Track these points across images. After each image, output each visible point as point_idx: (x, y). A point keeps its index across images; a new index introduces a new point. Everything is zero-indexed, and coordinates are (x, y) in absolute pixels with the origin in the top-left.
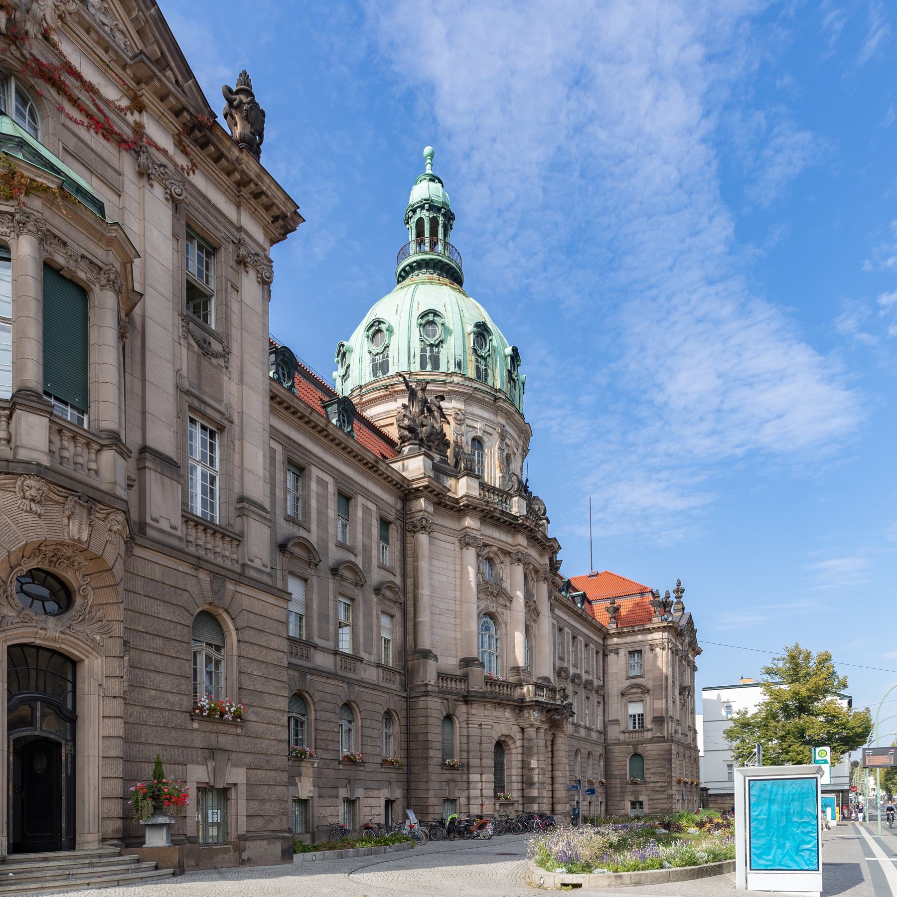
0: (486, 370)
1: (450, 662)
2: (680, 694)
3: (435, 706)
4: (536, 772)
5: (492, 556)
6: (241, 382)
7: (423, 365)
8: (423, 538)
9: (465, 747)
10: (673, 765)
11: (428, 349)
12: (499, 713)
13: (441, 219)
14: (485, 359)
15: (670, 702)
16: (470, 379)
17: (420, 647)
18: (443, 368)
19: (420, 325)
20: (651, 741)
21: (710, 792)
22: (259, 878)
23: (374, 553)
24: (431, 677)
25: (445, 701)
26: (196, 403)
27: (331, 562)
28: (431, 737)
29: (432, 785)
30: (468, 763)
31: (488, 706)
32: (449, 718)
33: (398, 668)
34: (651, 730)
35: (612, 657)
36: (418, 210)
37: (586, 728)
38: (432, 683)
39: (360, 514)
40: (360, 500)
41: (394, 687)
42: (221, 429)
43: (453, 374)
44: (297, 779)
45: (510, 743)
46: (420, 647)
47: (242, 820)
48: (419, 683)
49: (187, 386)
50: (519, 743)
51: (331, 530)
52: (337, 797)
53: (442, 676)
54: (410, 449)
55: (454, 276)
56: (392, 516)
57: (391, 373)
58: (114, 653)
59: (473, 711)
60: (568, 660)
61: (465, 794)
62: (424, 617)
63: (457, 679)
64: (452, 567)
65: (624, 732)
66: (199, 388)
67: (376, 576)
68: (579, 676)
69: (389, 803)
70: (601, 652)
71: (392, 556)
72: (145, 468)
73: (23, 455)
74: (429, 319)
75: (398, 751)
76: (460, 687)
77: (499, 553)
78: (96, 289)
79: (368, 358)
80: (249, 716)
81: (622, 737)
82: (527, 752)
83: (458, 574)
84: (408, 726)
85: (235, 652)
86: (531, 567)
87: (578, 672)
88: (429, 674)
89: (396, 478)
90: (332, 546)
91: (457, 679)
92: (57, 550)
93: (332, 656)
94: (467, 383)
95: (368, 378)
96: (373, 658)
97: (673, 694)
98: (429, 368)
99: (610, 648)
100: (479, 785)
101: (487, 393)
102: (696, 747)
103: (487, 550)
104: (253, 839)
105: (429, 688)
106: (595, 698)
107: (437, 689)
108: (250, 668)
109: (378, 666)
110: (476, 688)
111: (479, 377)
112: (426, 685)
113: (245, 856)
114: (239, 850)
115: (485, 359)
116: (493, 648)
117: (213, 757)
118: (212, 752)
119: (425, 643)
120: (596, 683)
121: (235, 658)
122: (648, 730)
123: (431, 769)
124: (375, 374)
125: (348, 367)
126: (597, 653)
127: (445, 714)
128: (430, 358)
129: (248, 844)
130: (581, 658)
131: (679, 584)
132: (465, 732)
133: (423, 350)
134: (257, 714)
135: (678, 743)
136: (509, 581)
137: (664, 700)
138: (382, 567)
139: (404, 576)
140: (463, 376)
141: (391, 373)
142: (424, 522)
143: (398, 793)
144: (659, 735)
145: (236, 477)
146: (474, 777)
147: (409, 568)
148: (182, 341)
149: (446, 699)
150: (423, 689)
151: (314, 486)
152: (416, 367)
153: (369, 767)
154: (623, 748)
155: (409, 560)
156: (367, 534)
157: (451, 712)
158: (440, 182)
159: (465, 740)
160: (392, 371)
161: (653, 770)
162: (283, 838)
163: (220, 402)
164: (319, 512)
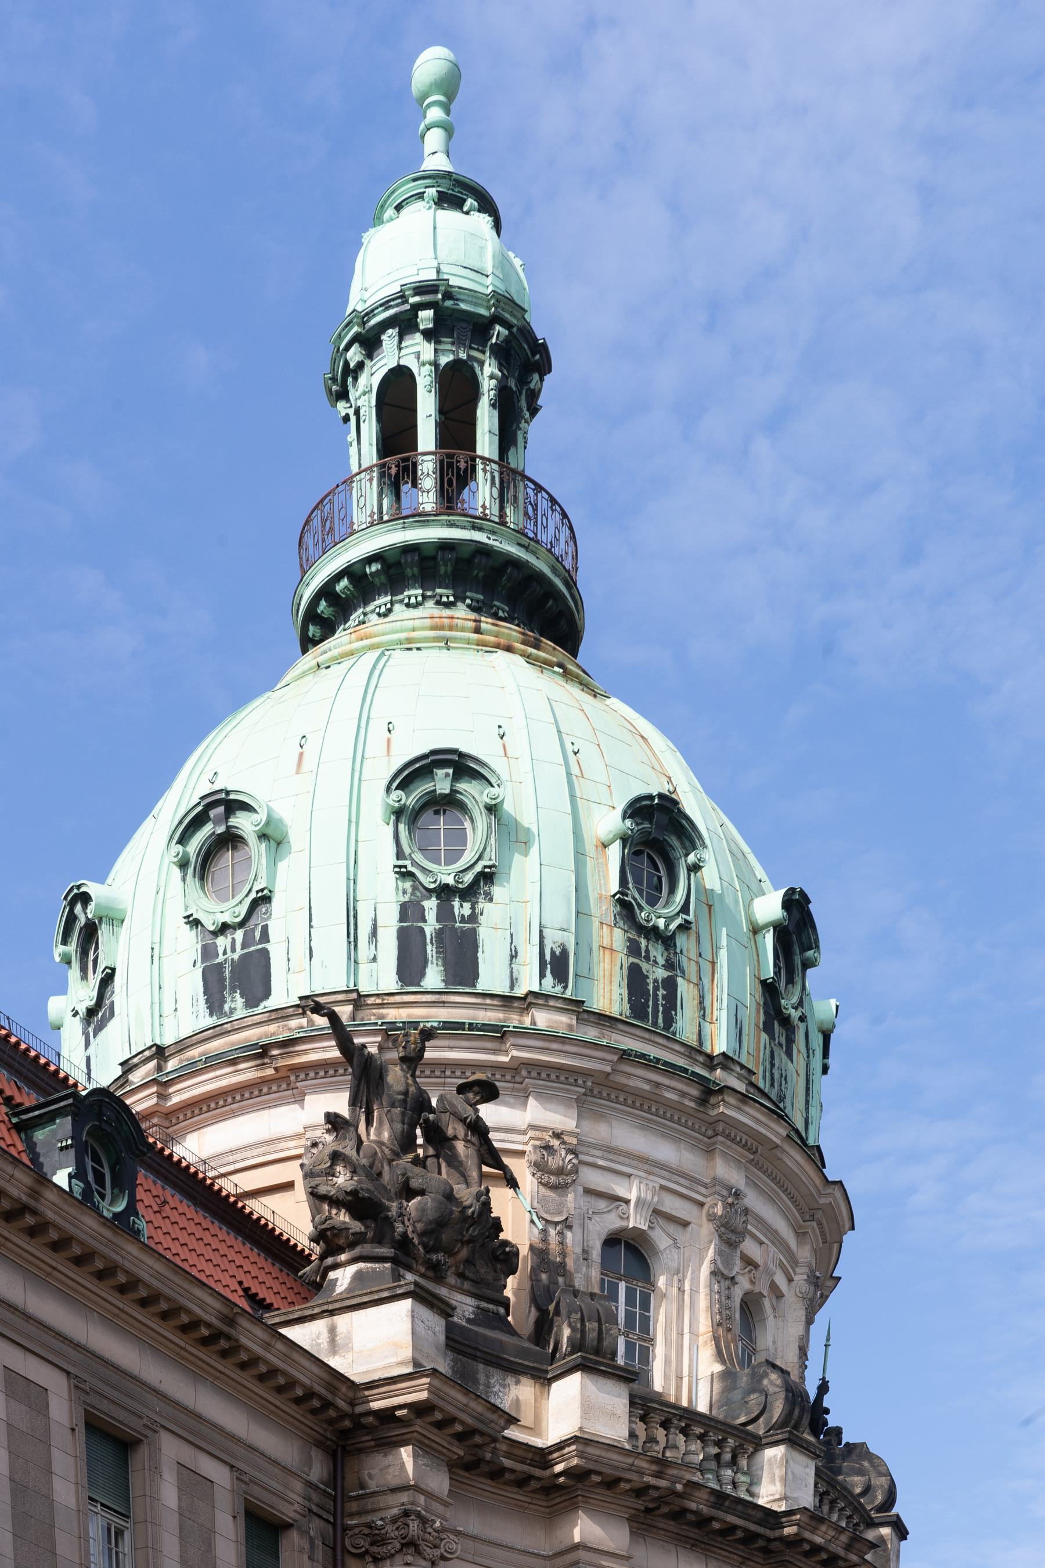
0: (670, 984)
7: (410, 969)
11: (431, 905)
18: (492, 976)
36: (390, 338)
39: (169, 1495)
40: (171, 1449)
54: (358, 1277)
95: (186, 1015)
98: (433, 978)
101: (671, 1070)
115: (668, 941)
125: (108, 979)
128: (442, 931)
133: (410, 912)
140: (576, 1007)
142: (414, 1526)
152: (381, 975)
160: (284, 992)
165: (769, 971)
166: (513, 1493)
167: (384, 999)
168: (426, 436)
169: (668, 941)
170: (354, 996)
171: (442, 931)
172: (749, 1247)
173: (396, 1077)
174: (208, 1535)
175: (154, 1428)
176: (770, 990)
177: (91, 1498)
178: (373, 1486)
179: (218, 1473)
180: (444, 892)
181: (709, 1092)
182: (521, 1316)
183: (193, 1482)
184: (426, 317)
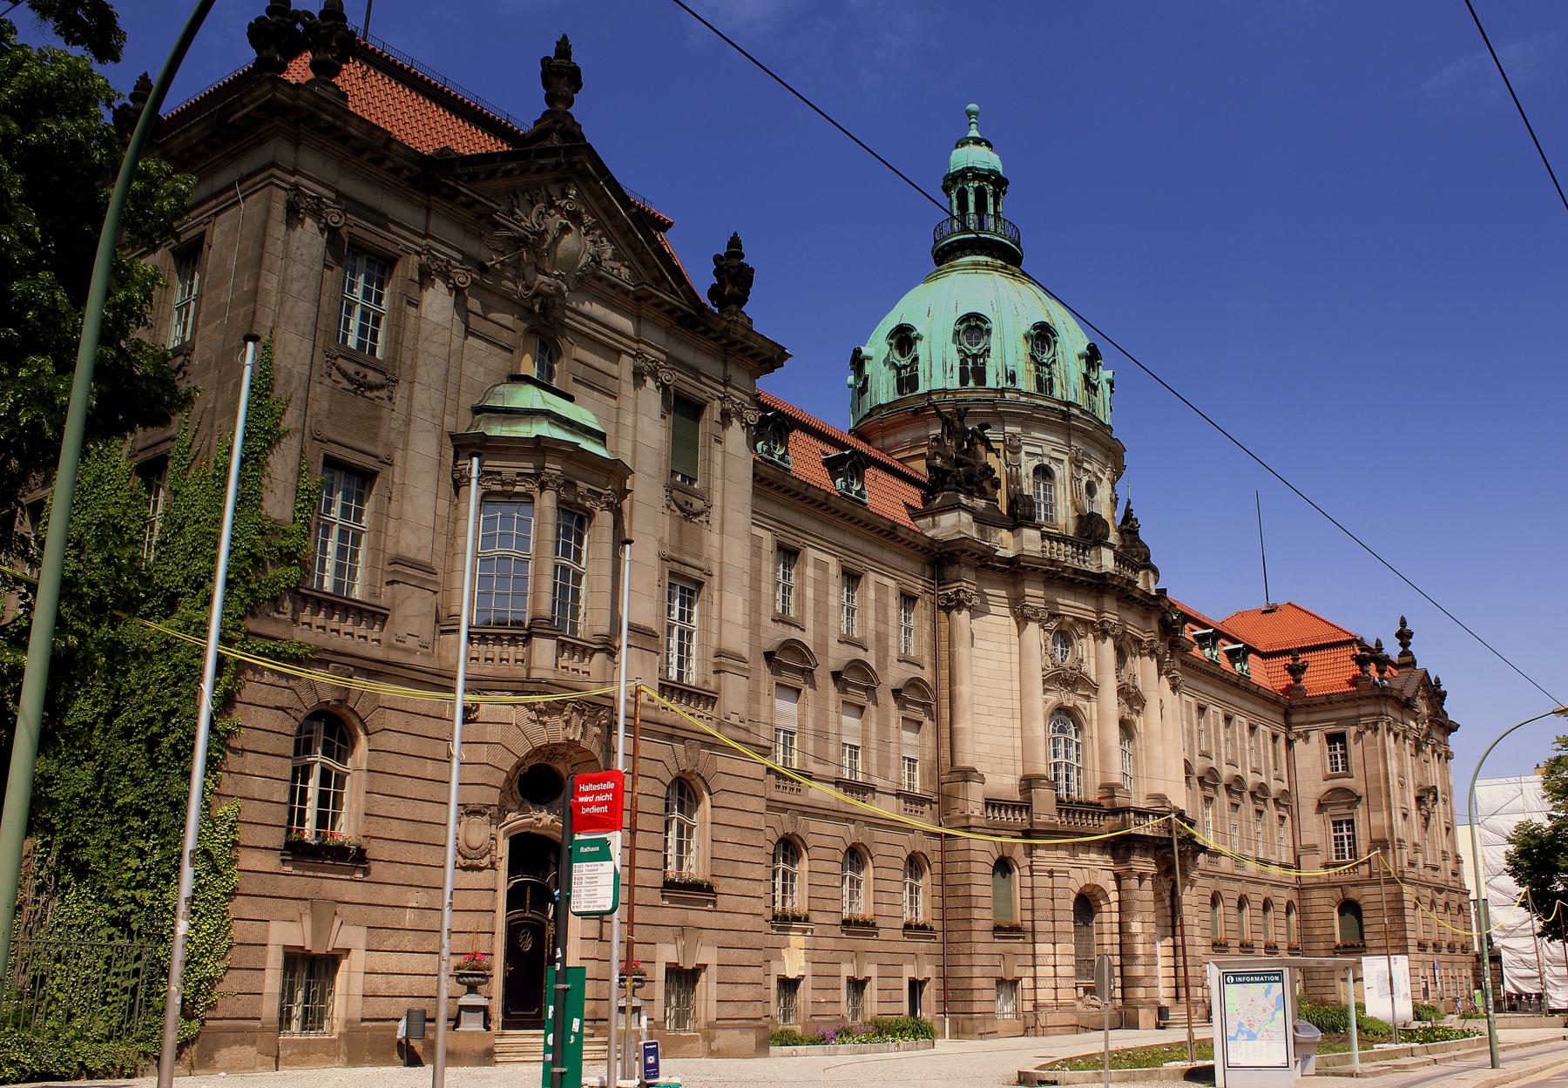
0: (1051, 380)
1: (1005, 783)
2: (1419, 800)
4: (1140, 939)
6: (722, 532)
7: (964, 381)
10: (1408, 920)
11: (970, 361)
15: (1397, 816)
16: (1027, 394)
17: (960, 764)
18: (991, 382)
23: (892, 641)
24: (975, 808)
26: (676, 566)
28: (975, 890)
37: (1258, 860)
38: (977, 813)
39: (872, 594)
42: (700, 584)
43: (1003, 391)
46: (960, 764)
47: (713, 1005)
49: (668, 552)
51: (833, 622)
53: (991, 804)
55: (1009, 257)
60: (1218, 755)
61: (1030, 972)
62: (964, 723)
64: (1005, 648)
66: (680, 549)
67: (896, 674)
68: (1239, 780)
69: (916, 986)
70: (1283, 736)
71: (918, 646)
73: (535, 674)
74: (973, 326)
75: (929, 909)
76: (1020, 819)
78: (597, 511)
80: (721, 886)
82: (1124, 908)
83: (1016, 658)
85: (709, 819)
87: (1239, 772)
88: (973, 799)
89: (921, 542)
92: (551, 751)
94: (1023, 399)
97: (1403, 800)
98: (971, 384)
100: (1051, 960)
102: (1462, 884)
106: (1272, 812)
107: (984, 822)
108: (725, 834)
109: (898, 795)
110: (1044, 819)
111: (1040, 389)
112: (968, 817)
113: (714, 1046)
114: (709, 1039)
115: (1048, 366)
116: (1073, 760)
117: (683, 935)
118: (682, 929)
119: (966, 759)
120: (1275, 787)
124: (900, 391)
126: (1275, 738)
128: (973, 370)
129: (719, 1033)
130: (1243, 749)
131: (1403, 623)
132: (1027, 881)
133: (963, 362)
134: (730, 886)
135: (1418, 883)
136: (1093, 661)
137: (1385, 814)
138: (904, 660)
139: (936, 666)
140: (1019, 391)
142: (962, 595)
143: (928, 971)
145: (715, 630)
146: (1043, 948)
147: (944, 656)
148: (666, 510)
151: (810, 571)
152: (955, 383)
155: (944, 645)
156: (882, 617)
158: (989, 145)
160: (922, 389)
162: (757, 1028)
163: (699, 557)
164: (817, 601)
167: (955, 392)
168: (972, 208)
169: (1048, 366)
171: (973, 370)
173: (957, 424)
174: (886, 606)
176: (1086, 377)
180: (975, 357)
182: (1003, 506)
183: (881, 588)
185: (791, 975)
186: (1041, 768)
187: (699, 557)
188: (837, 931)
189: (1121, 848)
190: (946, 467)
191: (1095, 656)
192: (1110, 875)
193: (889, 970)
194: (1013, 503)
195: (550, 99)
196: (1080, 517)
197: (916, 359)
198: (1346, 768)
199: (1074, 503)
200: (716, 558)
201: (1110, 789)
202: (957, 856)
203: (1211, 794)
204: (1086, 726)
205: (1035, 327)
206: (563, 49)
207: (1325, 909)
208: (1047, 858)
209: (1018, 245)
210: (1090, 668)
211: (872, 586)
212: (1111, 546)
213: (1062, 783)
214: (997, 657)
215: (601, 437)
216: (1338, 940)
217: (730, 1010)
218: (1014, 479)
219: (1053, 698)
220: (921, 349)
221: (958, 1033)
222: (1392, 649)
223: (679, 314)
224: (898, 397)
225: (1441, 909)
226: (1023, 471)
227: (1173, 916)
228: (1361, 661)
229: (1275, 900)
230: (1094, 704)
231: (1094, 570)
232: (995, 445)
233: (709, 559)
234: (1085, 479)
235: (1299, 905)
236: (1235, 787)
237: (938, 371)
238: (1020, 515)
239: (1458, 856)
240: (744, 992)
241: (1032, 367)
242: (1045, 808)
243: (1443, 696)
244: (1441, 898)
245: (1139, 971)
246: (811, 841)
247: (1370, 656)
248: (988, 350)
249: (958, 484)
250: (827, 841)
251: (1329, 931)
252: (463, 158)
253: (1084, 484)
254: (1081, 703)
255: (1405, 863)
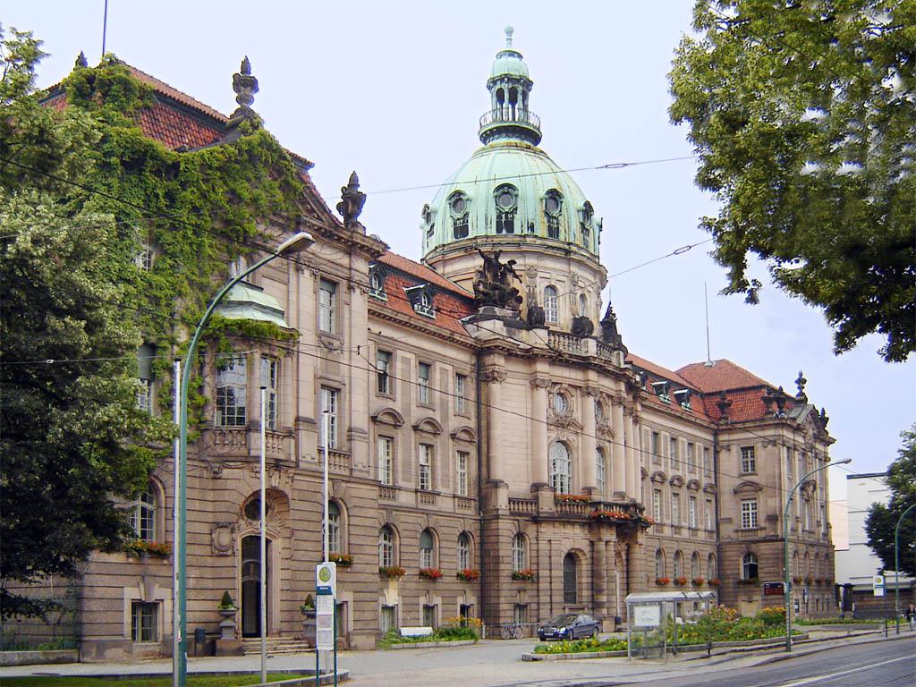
1: (520, 487)
3: (506, 527)
5: (562, 391)
7: (499, 230)
8: (495, 387)
9: (534, 560)
11: (503, 215)
12: (569, 530)
13: (520, 89)
14: (557, 219)
16: (542, 238)
18: (517, 231)
19: (496, 197)
20: (765, 541)
21: (854, 589)
22: (663, 369)
25: (516, 522)
26: (325, 382)
27: (413, 422)
29: (503, 593)
30: (538, 573)
31: (557, 525)
32: (520, 536)
33: (472, 496)
34: (765, 529)
35: (723, 455)
36: (499, 82)
38: (503, 507)
40: (438, 365)
41: (469, 512)
43: (525, 236)
44: (385, 591)
45: (580, 555)
46: (492, 478)
48: (491, 508)
49: (319, 373)
50: (588, 555)
52: (418, 604)
54: (484, 310)
56: (467, 370)
57: (470, 236)
58: (286, 536)
59: (542, 530)
63: (527, 502)
65: (737, 531)
67: (454, 424)
69: (464, 609)
70: (712, 448)
72: (298, 429)
77: (570, 389)
79: (450, 223)
81: (734, 536)
84: (482, 543)
86: (604, 395)
88: (501, 500)
90: (413, 407)
91: (527, 502)
93: (414, 494)
94: (539, 242)
95: (450, 239)
96: (450, 491)
98: (504, 232)
99: (721, 444)
101: (559, 249)
103: (558, 387)
104: (358, 634)
105: (500, 512)
110: (546, 509)
111: (551, 235)
112: (498, 510)
116: (566, 473)
121: (346, 526)
122: (761, 529)
123: (502, 580)
125: (432, 226)
127: (515, 533)
128: (505, 223)
131: (801, 375)
132: (534, 547)
133: (499, 217)
136: (580, 411)
137: (777, 498)
140: (536, 237)
141: (470, 236)
143: (472, 600)
144: (772, 533)
149: (517, 520)
150: (495, 513)
152: (493, 232)
153: (445, 579)
154: (735, 547)
157: (522, 531)
159: (534, 554)
161: (766, 570)
165: (582, 221)
166: (522, 359)
170: (376, 632)
171: (505, 223)
172: (580, 284)
175: (434, 361)
176: (582, 224)
177: (520, 56)
178: (486, 364)
179: (449, 368)
181: (568, 252)
182: (524, 315)
183: (444, 371)
184: (506, 79)
185: (391, 605)
186: (545, 479)
187: (338, 375)
188: (416, 578)
189: (595, 523)
190: (486, 291)
191: (585, 410)
192: (587, 542)
193: (449, 599)
194: (530, 312)
195: (239, 100)
196: (575, 318)
197: (467, 215)
198: (753, 470)
199: (571, 309)
200: (347, 374)
201: (589, 490)
202: (490, 533)
203: (659, 487)
204: (574, 451)
205: (548, 193)
206: (246, 66)
207: (735, 558)
208: (547, 531)
209: (538, 129)
210: (577, 416)
211: (438, 371)
212: (595, 338)
213: (558, 486)
214: (516, 405)
215: (281, 313)
216: (742, 578)
217: (360, 625)
218: (532, 295)
219: (554, 435)
220: (470, 208)
221: (491, 636)
222: (792, 391)
223: (323, 230)
224: (454, 240)
225: (802, 557)
226: (537, 290)
227: (628, 565)
228: (767, 401)
229: (701, 553)
230: (580, 439)
231: (584, 355)
232: (517, 273)
233: (343, 377)
234: (579, 292)
235: (719, 555)
236: (677, 482)
237: (482, 223)
238: (536, 319)
239: (828, 524)
240: (368, 616)
241: (546, 219)
242: (547, 504)
243: (825, 420)
244: (813, 551)
245: (604, 599)
246: (401, 527)
247: (778, 397)
248: (516, 209)
249: (495, 302)
250: (411, 527)
251: (736, 572)
252: (275, 297)
253: (578, 296)
254: (572, 437)
255: (789, 528)
